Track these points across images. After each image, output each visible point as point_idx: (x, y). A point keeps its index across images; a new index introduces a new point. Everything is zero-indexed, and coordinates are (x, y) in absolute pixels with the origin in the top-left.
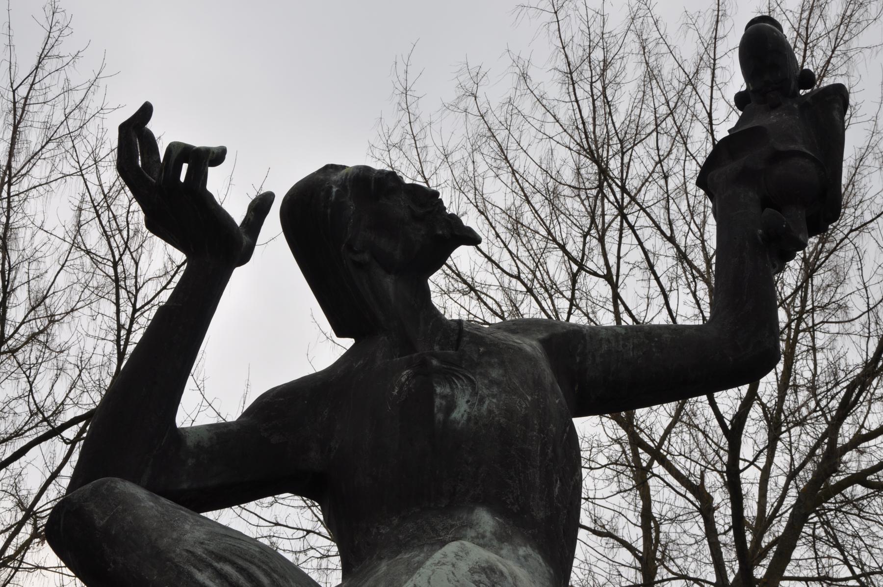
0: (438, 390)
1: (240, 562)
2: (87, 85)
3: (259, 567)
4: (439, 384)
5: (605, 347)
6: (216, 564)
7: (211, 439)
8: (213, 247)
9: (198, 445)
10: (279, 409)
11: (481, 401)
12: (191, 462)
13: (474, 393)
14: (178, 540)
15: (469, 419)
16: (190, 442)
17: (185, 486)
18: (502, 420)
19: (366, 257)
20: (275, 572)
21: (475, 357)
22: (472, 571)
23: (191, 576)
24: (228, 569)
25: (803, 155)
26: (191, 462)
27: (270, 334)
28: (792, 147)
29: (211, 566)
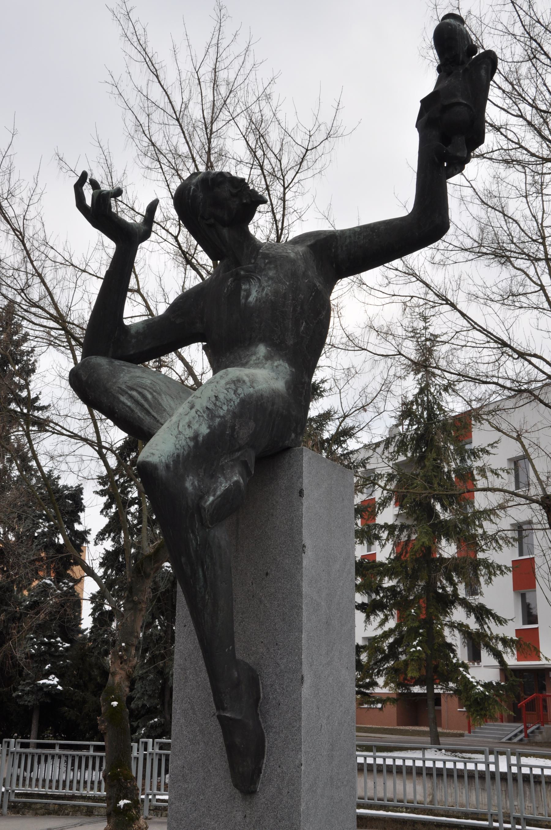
0: (243, 287)
1: (140, 390)
2: (244, 52)
3: (148, 391)
4: (244, 284)
5: (348, 241)
6: (129, 392)
7: (144, 328)
8: (127, 238)
9: (137, 332)
10: (186, 303)
11: (263, 290)
12: (134, 341)
13: (260, 286)
14: (116, 382)
15: (256, 300)
16: (133, 331)
17: (132, 352)
18: (273, 298)
19: (212, 221)
20: (155, 391)
21: (263, 265)
22: (227, 383)
23: (118, 399)
24: (134, 393)
25: (459, 104)
26: (134, 341)
27: (165, 273)
28: (454, 100)
29: (127, 393)
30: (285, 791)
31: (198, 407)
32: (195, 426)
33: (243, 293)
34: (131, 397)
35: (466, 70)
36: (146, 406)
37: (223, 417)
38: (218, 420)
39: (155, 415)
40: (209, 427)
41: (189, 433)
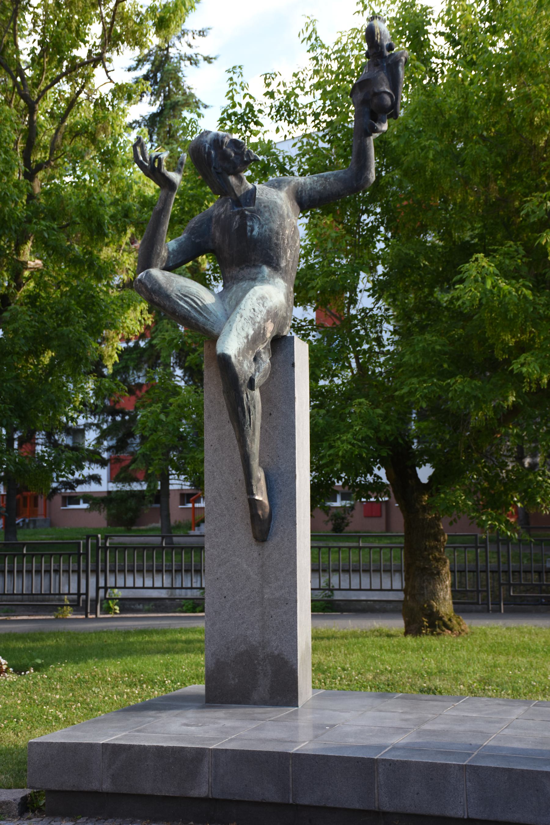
11: (262, 227)
13: (260, 224)
30: (286, 539)
31: (245, 316)
32: (246, 329)
33: (249, 228)
34: (186, 302)
35: (388, 65)
36: (199, 309)
37: (259, 323)
38: (257, 325)
39: (205, 314)
40: (253, 330)
41: (244, 334)
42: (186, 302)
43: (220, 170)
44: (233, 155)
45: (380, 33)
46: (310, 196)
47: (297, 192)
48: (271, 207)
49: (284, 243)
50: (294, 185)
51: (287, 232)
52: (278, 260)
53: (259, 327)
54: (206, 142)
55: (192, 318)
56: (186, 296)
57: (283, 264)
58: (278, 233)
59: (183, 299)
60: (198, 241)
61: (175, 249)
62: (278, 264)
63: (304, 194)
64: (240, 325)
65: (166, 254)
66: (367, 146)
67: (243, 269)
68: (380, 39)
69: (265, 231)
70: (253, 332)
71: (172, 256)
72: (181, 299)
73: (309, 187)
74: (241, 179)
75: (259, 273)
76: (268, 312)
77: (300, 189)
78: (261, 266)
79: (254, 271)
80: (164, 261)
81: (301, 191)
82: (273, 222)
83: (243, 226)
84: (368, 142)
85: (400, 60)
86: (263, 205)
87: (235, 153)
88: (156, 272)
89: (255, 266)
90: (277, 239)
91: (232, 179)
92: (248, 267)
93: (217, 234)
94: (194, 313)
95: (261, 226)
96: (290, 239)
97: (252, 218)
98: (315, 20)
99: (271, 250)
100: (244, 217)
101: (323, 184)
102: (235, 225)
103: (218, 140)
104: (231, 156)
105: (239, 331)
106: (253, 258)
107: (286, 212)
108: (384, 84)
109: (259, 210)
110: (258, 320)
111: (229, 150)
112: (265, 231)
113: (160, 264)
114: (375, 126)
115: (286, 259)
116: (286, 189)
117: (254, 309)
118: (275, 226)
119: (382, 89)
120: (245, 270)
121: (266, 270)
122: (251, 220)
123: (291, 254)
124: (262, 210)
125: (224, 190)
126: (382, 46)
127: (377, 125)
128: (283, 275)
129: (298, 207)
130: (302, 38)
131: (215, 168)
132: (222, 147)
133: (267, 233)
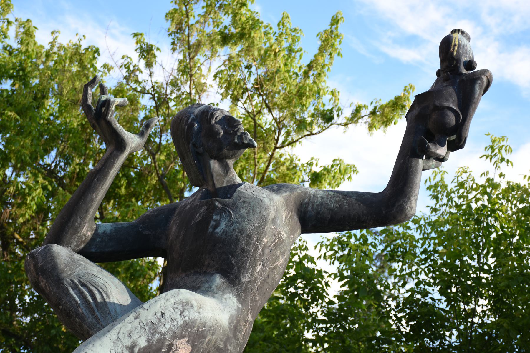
11: (232, 225)
13: (230, 220)
31: (143, 318)
32: (135, 336)
33: (212, 223)
34: (80, 294)
36: (93, 305)
37: (163, 334)
38: (157, 336)
39: (98, 314)
40: (148, 341)
42: (80, 294)
43: (201, 150)
44: (222, 133)
45: (459, 45)
46: (318, 213)
47: (301, 204)
48: (252, 204)
49: (256, 251)
50: (299, 194)
51: (265, 240)
52: (239, 271)
53: (161, 342)
54: (193, 113)
55: (78, 314)
56: (83, 285)
57: (245, 279)
58: (250, 237)
59: (78, 287)
60: (146, 232)
61: (108, 232)
62: (238, 277)
63: (310, 208)
64: (129, 327)
65: (89, 234)
66: (411, 167)
67: (188, 275)
68: (458, 51)
69: (234, 230)
70: (146, 344)
71: (98, 240)
72: (75, 287)
73: (320, 200)
74: (226, 169)
75: (207, 282)
76: (186, 325)
77: (306, 200)
78: (213, 274)
79: (202, 278)
80: (82, 242)
81: (307, 204)
82: (249, 221)
83: (207, 219)
84: (414, 163)
85: (481, 79)
86: (242, 200)
87: (225, 132)
88: (61, 252)
89: (205, 273)
90: (247, 244)
91: (215, 165)
92: (196, 273)
93: (174, 229)
94: (83, 310)
95: (231, 223)
96: (267, 251)
97: (223, 211)
98: (445, 172)
99: (233, 256)
100: (212, 209)
101: (340, 201)
102: (198, 217)
103: (207, 112)
104: (218, 133)
105: (120, 336)
106: (206, 263)
107: (272, 215)
108: (451, 100)
109: (234, 204)
110: (163, 330)
111: (218, 126)
112: (234, 230)
113: (75, 243)
114: (426, 144)
115: (253, 274)
116: (285, 194)
117: (163, 314)
118: (249, 227)
119: (446, 104)
120: (191, 276)
121: (218, 280)
122: (221, 214)
123: (262, 270)
124: (239, 205)
125: (200, 175)
126: (458, 60)
127: (431, 145)
128: (241, 292)
129: (299, 223)
130: (428, 184)
131: (194, 145)
132: (210, 122)
133: (235, 234)
